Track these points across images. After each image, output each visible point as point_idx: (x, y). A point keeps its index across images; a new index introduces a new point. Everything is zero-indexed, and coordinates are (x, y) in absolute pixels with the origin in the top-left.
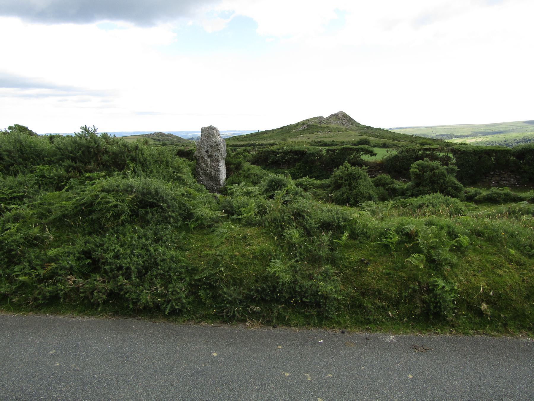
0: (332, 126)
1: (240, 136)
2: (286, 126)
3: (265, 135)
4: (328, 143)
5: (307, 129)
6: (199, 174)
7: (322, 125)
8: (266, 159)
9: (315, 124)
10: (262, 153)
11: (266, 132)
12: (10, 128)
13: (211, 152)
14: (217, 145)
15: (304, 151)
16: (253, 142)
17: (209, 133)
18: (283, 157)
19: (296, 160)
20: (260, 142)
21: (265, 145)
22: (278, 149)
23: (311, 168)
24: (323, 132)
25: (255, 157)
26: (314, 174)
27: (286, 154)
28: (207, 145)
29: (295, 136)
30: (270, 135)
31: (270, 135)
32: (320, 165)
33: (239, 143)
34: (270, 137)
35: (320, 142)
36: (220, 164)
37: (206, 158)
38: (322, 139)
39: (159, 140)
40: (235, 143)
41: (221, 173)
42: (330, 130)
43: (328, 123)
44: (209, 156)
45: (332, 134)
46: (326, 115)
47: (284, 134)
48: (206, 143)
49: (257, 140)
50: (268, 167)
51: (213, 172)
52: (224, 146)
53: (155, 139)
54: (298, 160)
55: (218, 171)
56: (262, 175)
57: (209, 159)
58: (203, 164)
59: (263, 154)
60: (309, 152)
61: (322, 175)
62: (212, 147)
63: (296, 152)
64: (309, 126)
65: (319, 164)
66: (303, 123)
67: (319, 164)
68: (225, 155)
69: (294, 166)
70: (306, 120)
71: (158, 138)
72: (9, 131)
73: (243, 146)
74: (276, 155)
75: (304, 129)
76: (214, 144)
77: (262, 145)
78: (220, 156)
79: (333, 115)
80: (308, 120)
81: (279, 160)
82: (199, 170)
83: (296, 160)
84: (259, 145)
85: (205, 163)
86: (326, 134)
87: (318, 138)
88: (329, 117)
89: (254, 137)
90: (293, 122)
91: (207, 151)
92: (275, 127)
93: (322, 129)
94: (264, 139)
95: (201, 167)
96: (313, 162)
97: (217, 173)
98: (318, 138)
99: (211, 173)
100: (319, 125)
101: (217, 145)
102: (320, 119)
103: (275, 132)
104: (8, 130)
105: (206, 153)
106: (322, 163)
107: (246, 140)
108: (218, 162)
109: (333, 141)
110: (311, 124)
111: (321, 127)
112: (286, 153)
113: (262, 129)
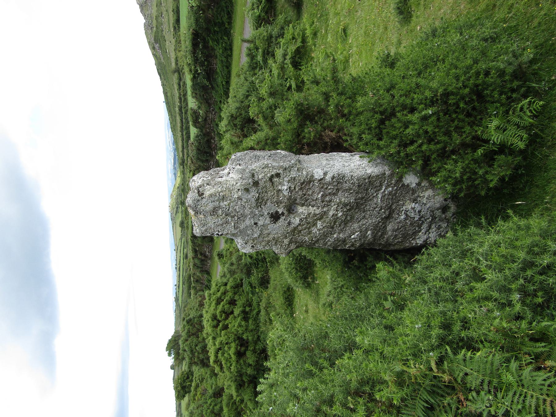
0: (155, 13)
1: (171, 123)
2: (158, 70)
3: (169, 94)
4: (175, 18)
5: (160, 44)
6: (344, 241)
7: (154, 26)
8: (204, 88)
9: (154, 34)
10: (196, 94)
11: (165, 93)
12: (170, 355)
13: (278, 203)
14: (256, 184)
15: (193, 34)
16: (177, 109)
17: (214, 211)
18: (202, 65)
19: (206, 47)
20: (177, 100)
21: (180, 95)
22: (191, 71)
23: (215, 24)
24: (162, 24)
25: (201, 103)
26: (225, 19)
27: (197, 60)
28: (254, 216)
29: (169, 58)
30: (168, 89)
31: (168, 89)
32: (212, 10)
33: (179, 125)
34: (171, 89)
35: (175, 28)
36: (318, 174)
37: (296, 221)
38: (171, 25)
39: (177, 208)
40: (179, 129)
41: (346, 171)
42: (160, 15)
43: (151, 17)
44: (290, 210)
45: (164, 13)
46: (141, 20)
47: (166, 73)
48: (248, 222)
49: (174, 104)
50: (215, 85)
51: (341, 197)
52: (257, 158)
53: (177, 212)
54: (205, 42)
55: (339, 181)
56: (247, 84)
57: (300, 209)
58: (314, 230)
59: (197, 92)
60: (194, 26)
61: (227, 7)
62: (260, 202)
63: (195, 45)
64: (157, 40)
65: (210, 12)
66: (153, 48)
67: (210, 12)
68: (281, 158)
69: (213, 49)
70: (149, 45)
71: (175, 209)
72: (173, 356)
73: (182, 120)
74: (198, 74)
75: (160, 48)
76: (254, 193)
77: (180, 99)
78: (293, 174)
79: (142, 11)
80: (149, 42)
81: (205, 70)
82: (330, 240)
83: (206, 47)
84: (180, 102)
85: (309, 222)
86: (165, 20)
87: (169, 30)
88: (144, 15)
89: (172, 107)
90: (152, 61)
91: (275, 217)
92: (159, 82)
93: (159, 25)
94: (173, 96)
95: (325, 236)
96: (208, 21)
97: (346, 186)
98: (169, 30)
99: (345, 205)
100: (155, 29)
101: (256, 184)
102: (148, 27)
103: (165, 83)
104: (171, 357)
105: (282, 222)
106: (209, 7)
107: (175, 117)
108: (310, 180)
109: (173, 11)
110: (153, 39)
111: (157, 26)
112: (196, 60)
113: (162, 98)
